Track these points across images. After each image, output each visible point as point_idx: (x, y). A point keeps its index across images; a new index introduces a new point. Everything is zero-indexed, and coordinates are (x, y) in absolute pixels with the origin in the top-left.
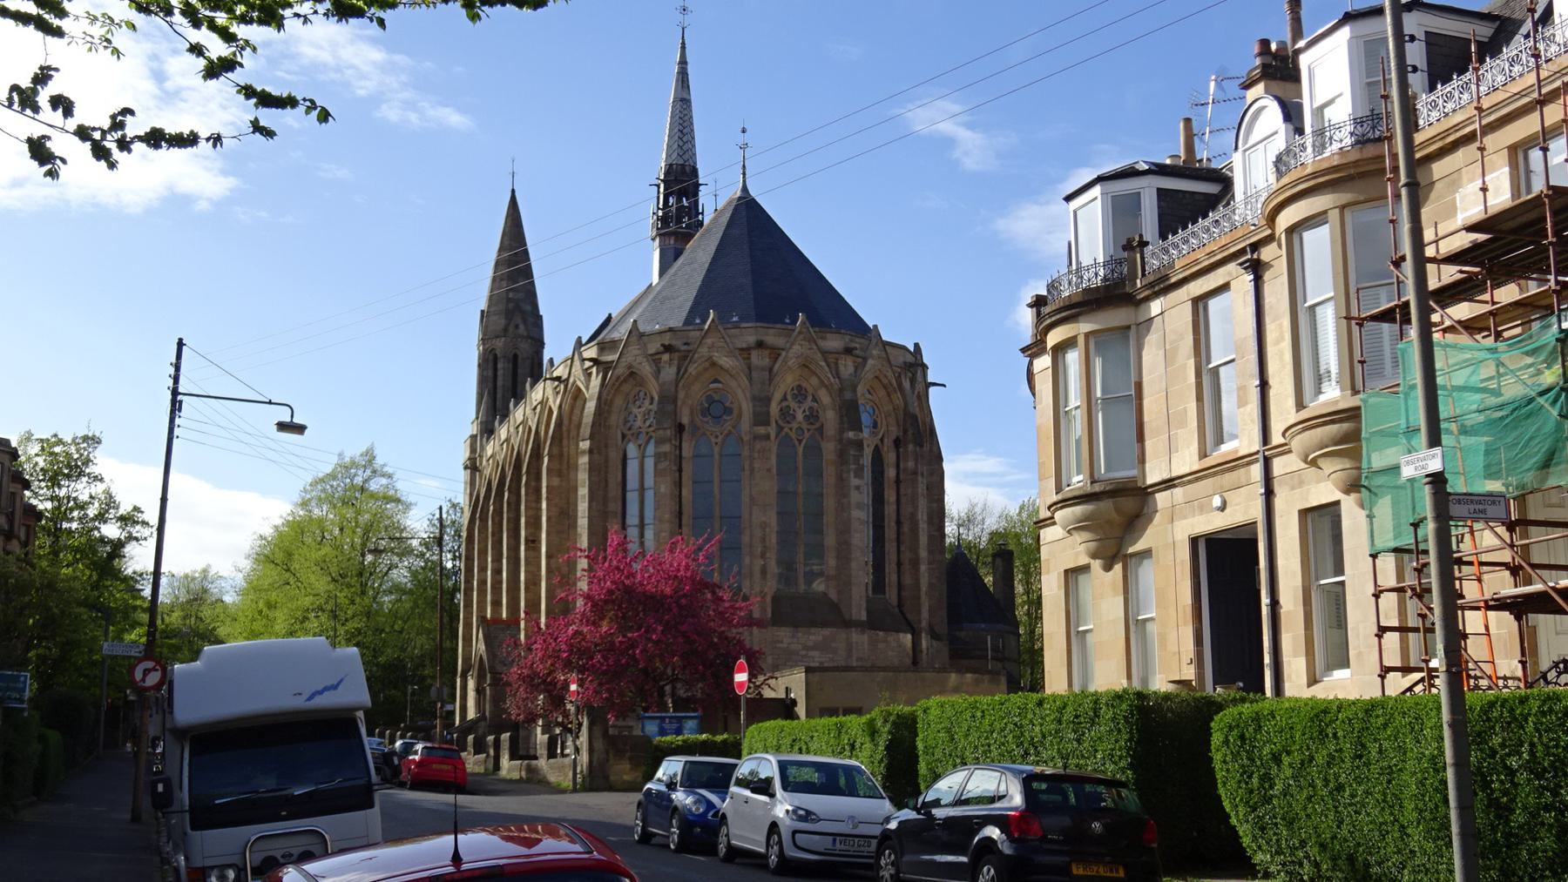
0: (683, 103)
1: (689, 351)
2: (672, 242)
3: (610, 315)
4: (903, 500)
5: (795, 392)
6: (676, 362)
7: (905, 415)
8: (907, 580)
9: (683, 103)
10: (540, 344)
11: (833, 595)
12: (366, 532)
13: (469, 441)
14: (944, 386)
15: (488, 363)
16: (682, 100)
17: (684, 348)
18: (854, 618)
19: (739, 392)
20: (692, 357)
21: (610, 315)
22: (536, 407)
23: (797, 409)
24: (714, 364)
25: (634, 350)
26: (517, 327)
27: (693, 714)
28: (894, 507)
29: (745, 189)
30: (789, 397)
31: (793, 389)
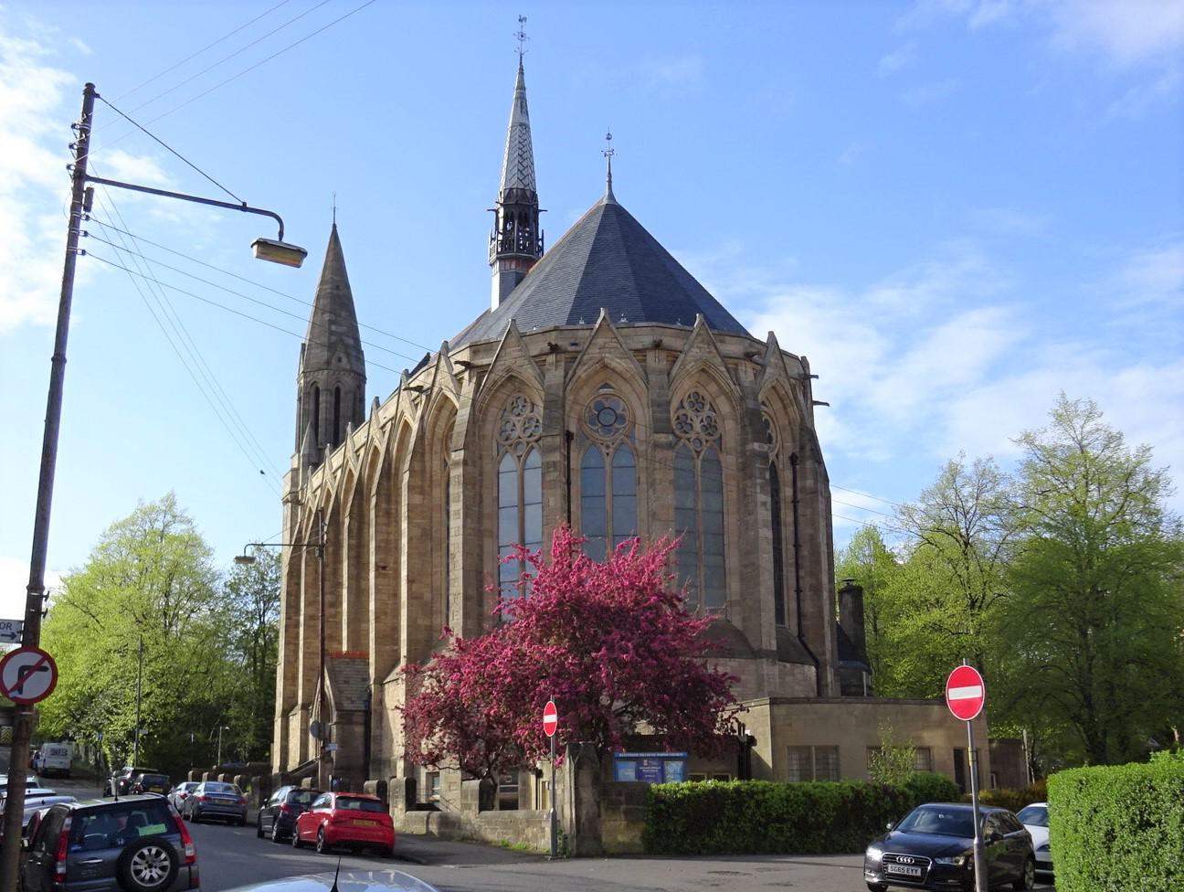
0: (522, 127)
1: (578, 352)
2: (513, 266)
3: (428, 354)
4: (801, 519)
5: (692, 399)
6: (563, 364)
7: (801, 430)
8: (808, 607)
9: (522, 127)
10: (361, 378)
11: (737, 622)
12: (171, 576)
13: (289, 476)
14: (827, 404)
15: (310, 396)
16: (521, 125)
17: (573, 348)
18: (764, 647)
19: (634, 398)
20: (582, 357)
21: (428, 354)
22: (385, 425)
23: (694, 418)
24: (605, 367)
25: (513, 352)
26: (340, 360)
27: (677, 755)
28: (792, 528)
29: (611, 196)
30: (686, 405)
31: (689, 396)
